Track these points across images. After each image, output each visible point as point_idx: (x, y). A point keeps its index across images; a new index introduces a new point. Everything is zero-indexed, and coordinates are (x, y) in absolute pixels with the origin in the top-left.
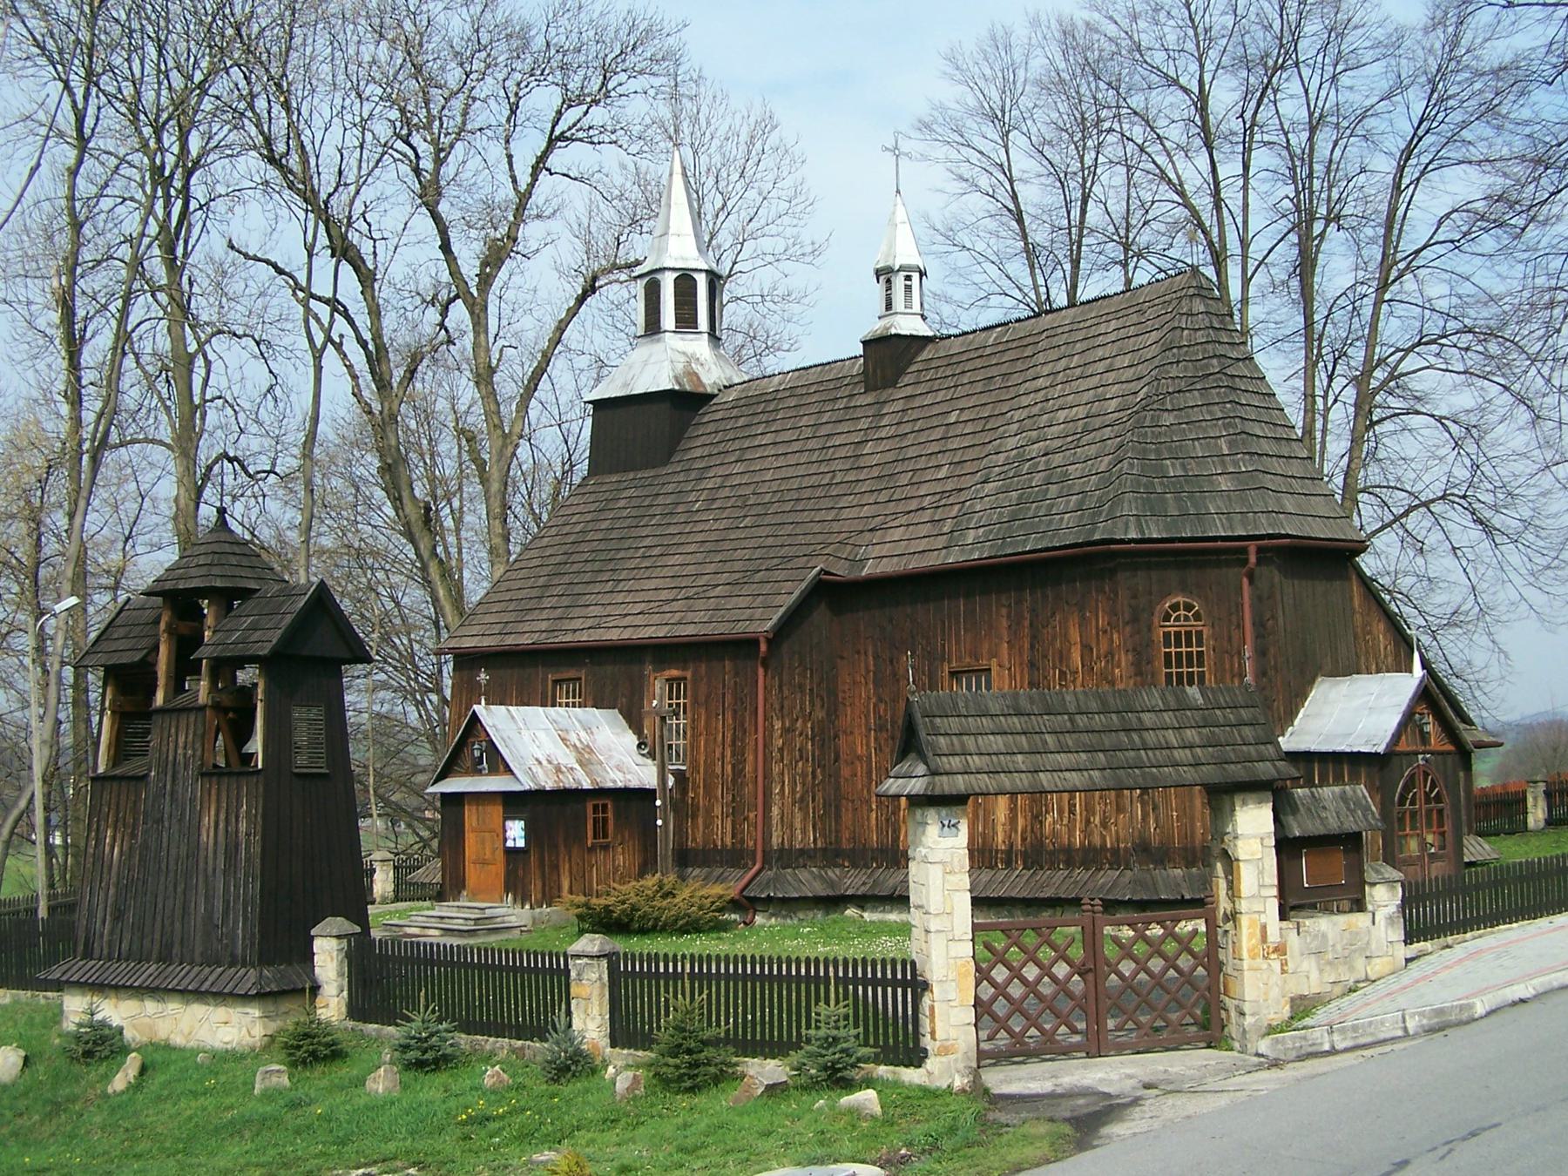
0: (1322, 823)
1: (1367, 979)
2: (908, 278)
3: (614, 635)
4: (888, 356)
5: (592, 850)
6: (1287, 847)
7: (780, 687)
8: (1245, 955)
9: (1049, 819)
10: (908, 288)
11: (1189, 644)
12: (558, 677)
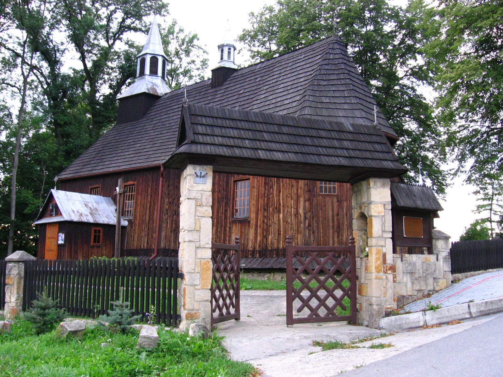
0: (414, 202)
1: (434, 290)
2: (230, 49)
3: (111, 170)
4: (222, 75)
5: (92, 247)
6: (398, 211)
7: (168, 186)
8: (374, 270)
9: (270, 237)
10: (229, 53)
11: (326, 187)
12: (92, 187)
